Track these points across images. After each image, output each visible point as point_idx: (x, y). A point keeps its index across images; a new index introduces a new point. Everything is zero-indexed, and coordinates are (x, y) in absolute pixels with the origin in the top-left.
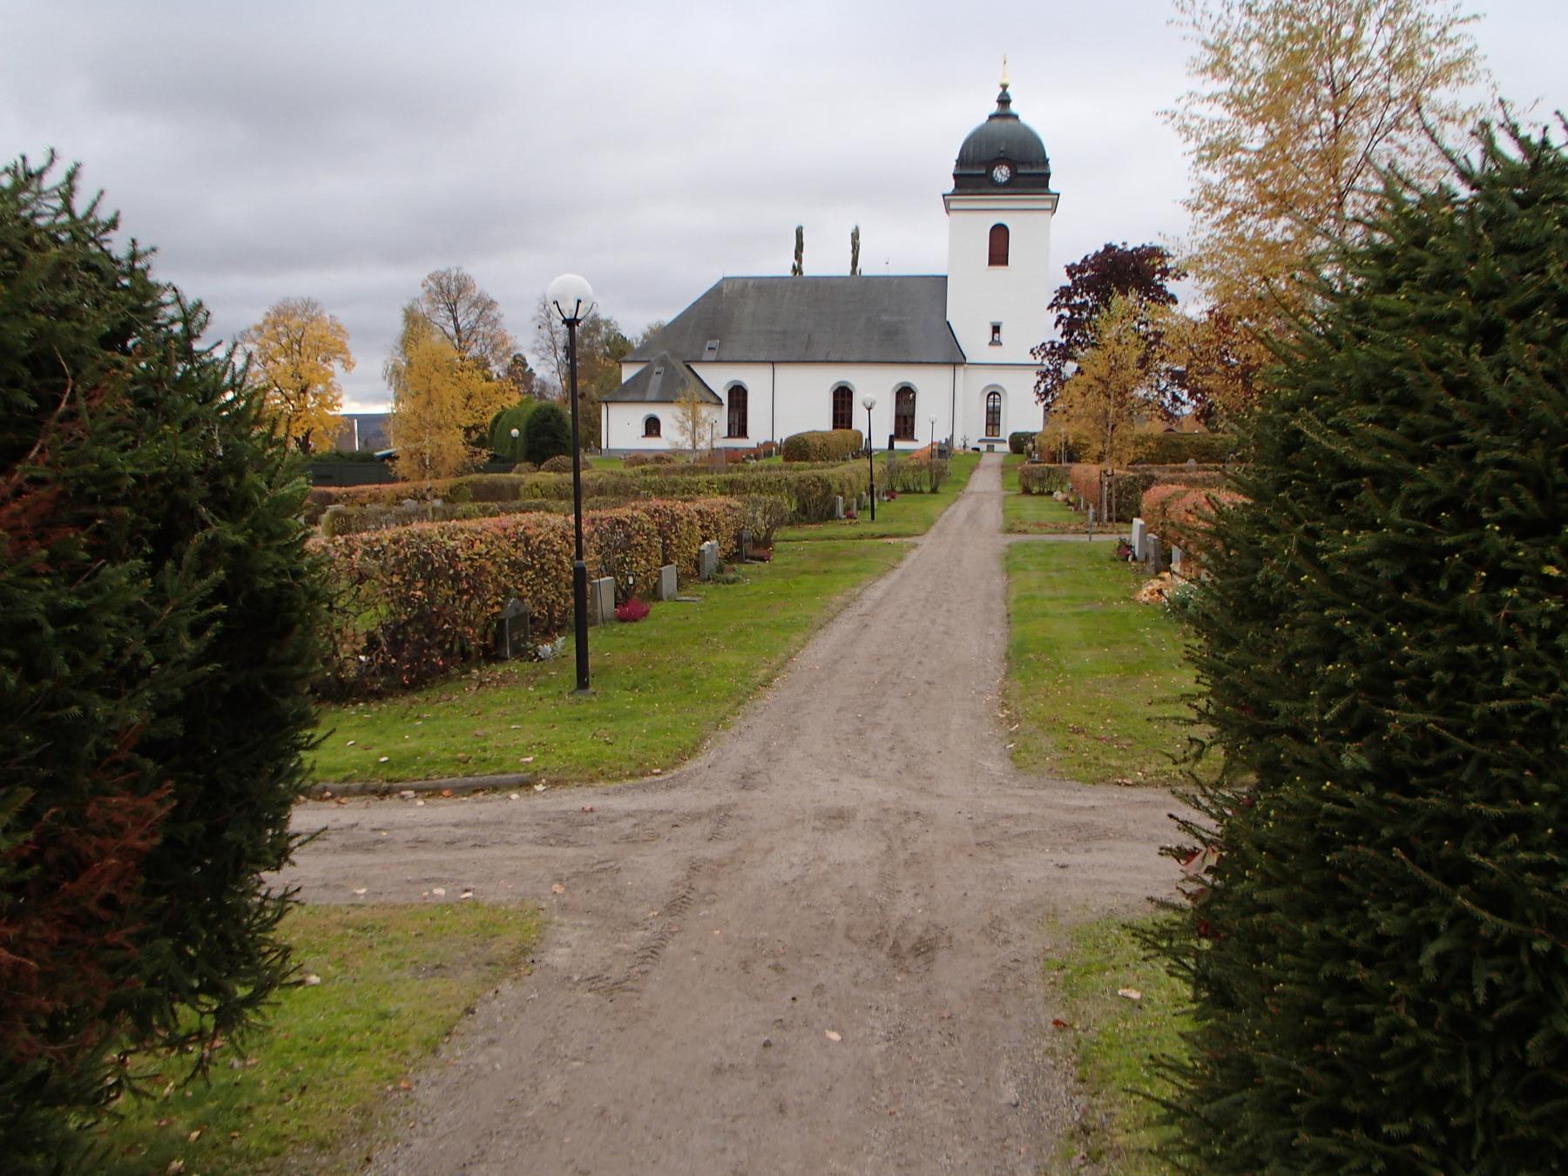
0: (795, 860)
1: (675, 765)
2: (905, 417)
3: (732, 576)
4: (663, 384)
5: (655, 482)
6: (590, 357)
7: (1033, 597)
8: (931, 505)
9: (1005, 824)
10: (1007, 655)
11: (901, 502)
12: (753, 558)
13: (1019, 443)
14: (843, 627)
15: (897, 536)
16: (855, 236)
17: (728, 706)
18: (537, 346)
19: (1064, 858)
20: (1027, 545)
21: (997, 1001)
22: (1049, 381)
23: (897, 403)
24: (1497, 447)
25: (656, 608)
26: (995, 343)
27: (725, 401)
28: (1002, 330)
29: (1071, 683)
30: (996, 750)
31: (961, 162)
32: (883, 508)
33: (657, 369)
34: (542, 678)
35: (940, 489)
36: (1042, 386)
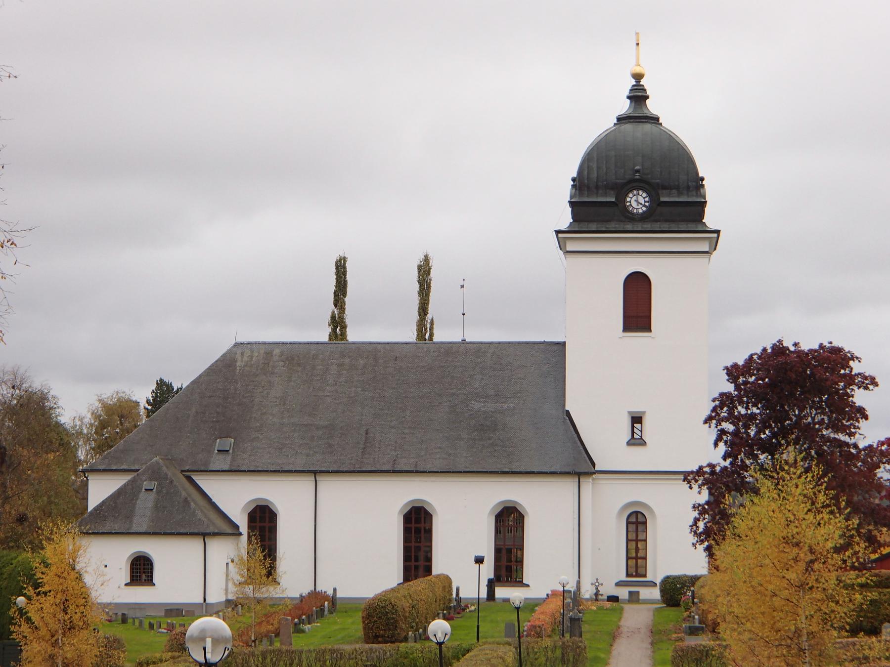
2: (509, 551)
4: (157, 507)
23: (497, 531)
26: (637, 441)
27: (244, 528)
28: (646, 421)
31: (580, 184)
33: (146, 485)
36: (701, 525)
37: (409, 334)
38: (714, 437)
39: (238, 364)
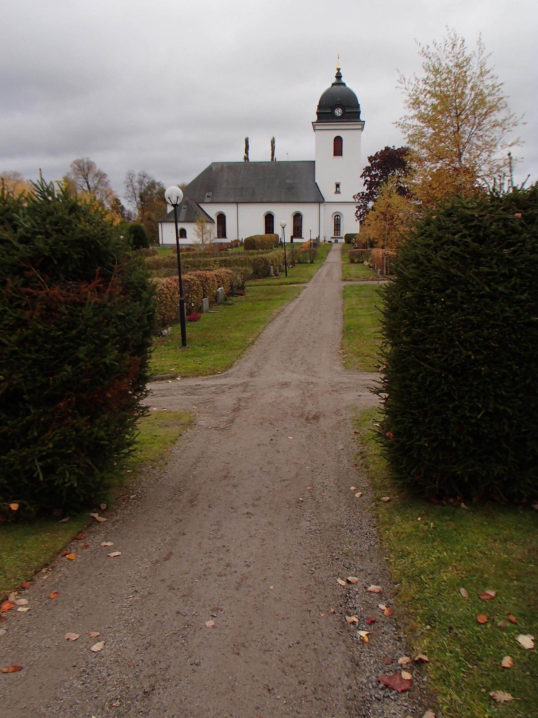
0: (272, 397)
1: (225, 371)
2: (298, 228)
3: (230, 302)
4: (187, 213)
5: (191, 261)
6: (151, 200)
7: (354, 308)
8: (311, 269)
9: (341, 385)
10: (343, 331)
11: (298, 267)
12: (238, 294)
13: (349, 238)
14: (279, 322)
15: (297, 283)
16: (273, 142)
17: (240, 351)
18: (127, 195)
19: (361, 394)
20: (352, 286)
21: (338, 429)
22: (361, 211)
24: (435, 274)
25: (204, 316)
26: (337, 192)
27: (216, 221)
28: (341, 186)
29: (366, 340)
30: (339, 363)
31: (319, 107)
32: (290, 271)
34: (165, 343)
35: (315, 261)
36: (359, 213)
37: (269, 159)
38: (364, 182)
39: (214, 169)
